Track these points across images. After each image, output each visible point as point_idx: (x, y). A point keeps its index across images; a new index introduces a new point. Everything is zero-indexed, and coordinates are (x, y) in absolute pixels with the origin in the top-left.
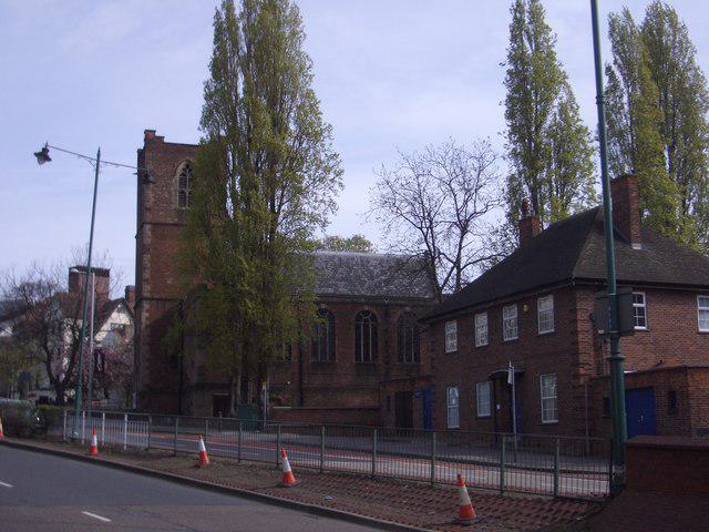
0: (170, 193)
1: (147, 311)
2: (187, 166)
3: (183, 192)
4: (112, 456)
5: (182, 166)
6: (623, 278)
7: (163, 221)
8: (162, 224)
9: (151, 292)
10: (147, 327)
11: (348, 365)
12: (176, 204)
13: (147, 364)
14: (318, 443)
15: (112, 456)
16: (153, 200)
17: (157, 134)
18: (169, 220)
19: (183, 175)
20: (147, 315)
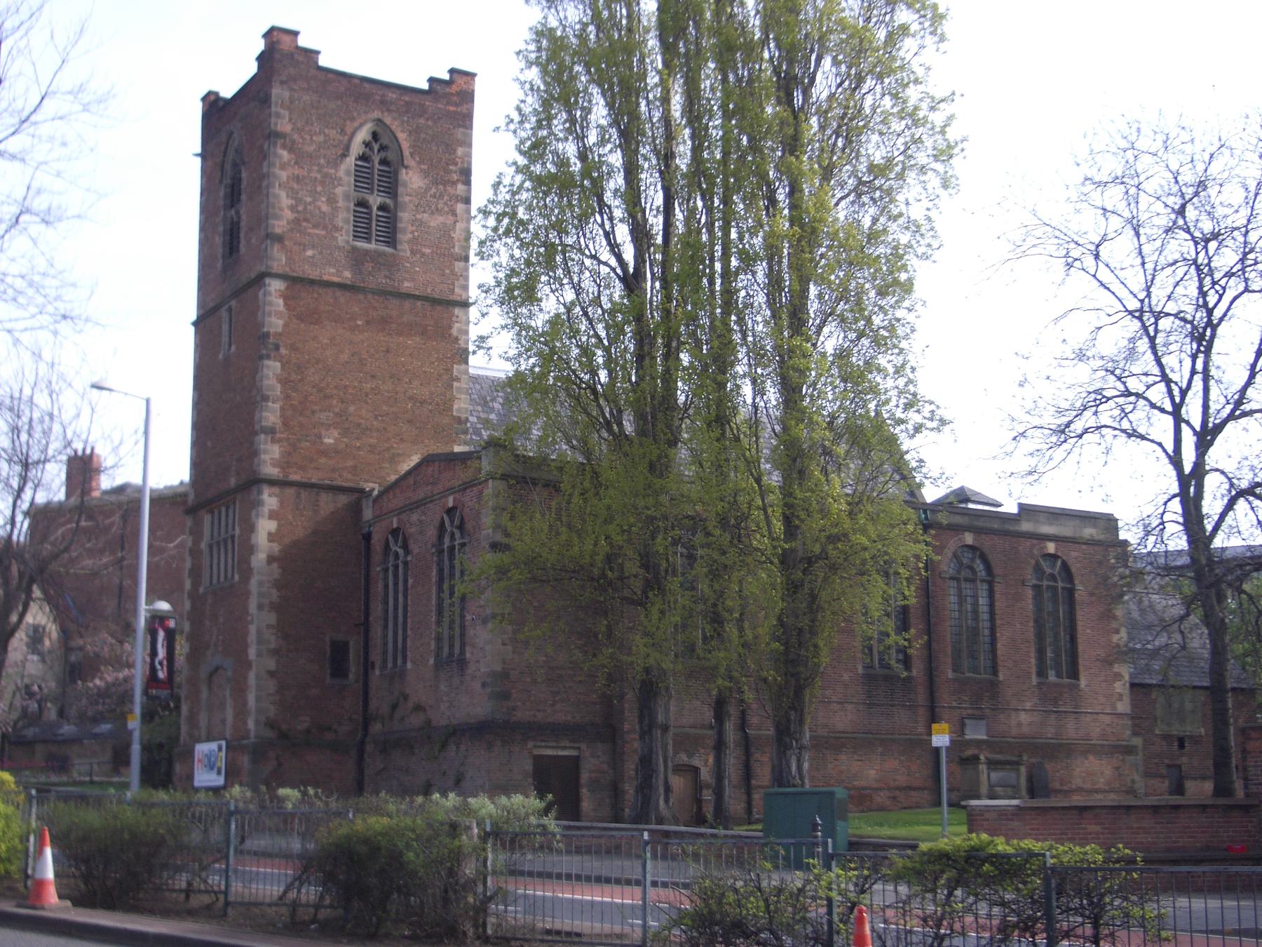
0: (332, 200)
1: (273, 515)
2: (375, 136)
3: (362, 204)
4: (42, 472)
5: (363, 135)
6: (1136, 681)
7: (313, 274)
8: (312, 282)
9: (285, 464)
10: (271, 559)
11: (846, 677)
12: (344, 237)
13: (271, 664)
14: (637, 875)
15: (42, 472)
16: (288, 215)
17: (302, 42)
18: (330, 274)
19: (363, 157)
20: (272, 526)
